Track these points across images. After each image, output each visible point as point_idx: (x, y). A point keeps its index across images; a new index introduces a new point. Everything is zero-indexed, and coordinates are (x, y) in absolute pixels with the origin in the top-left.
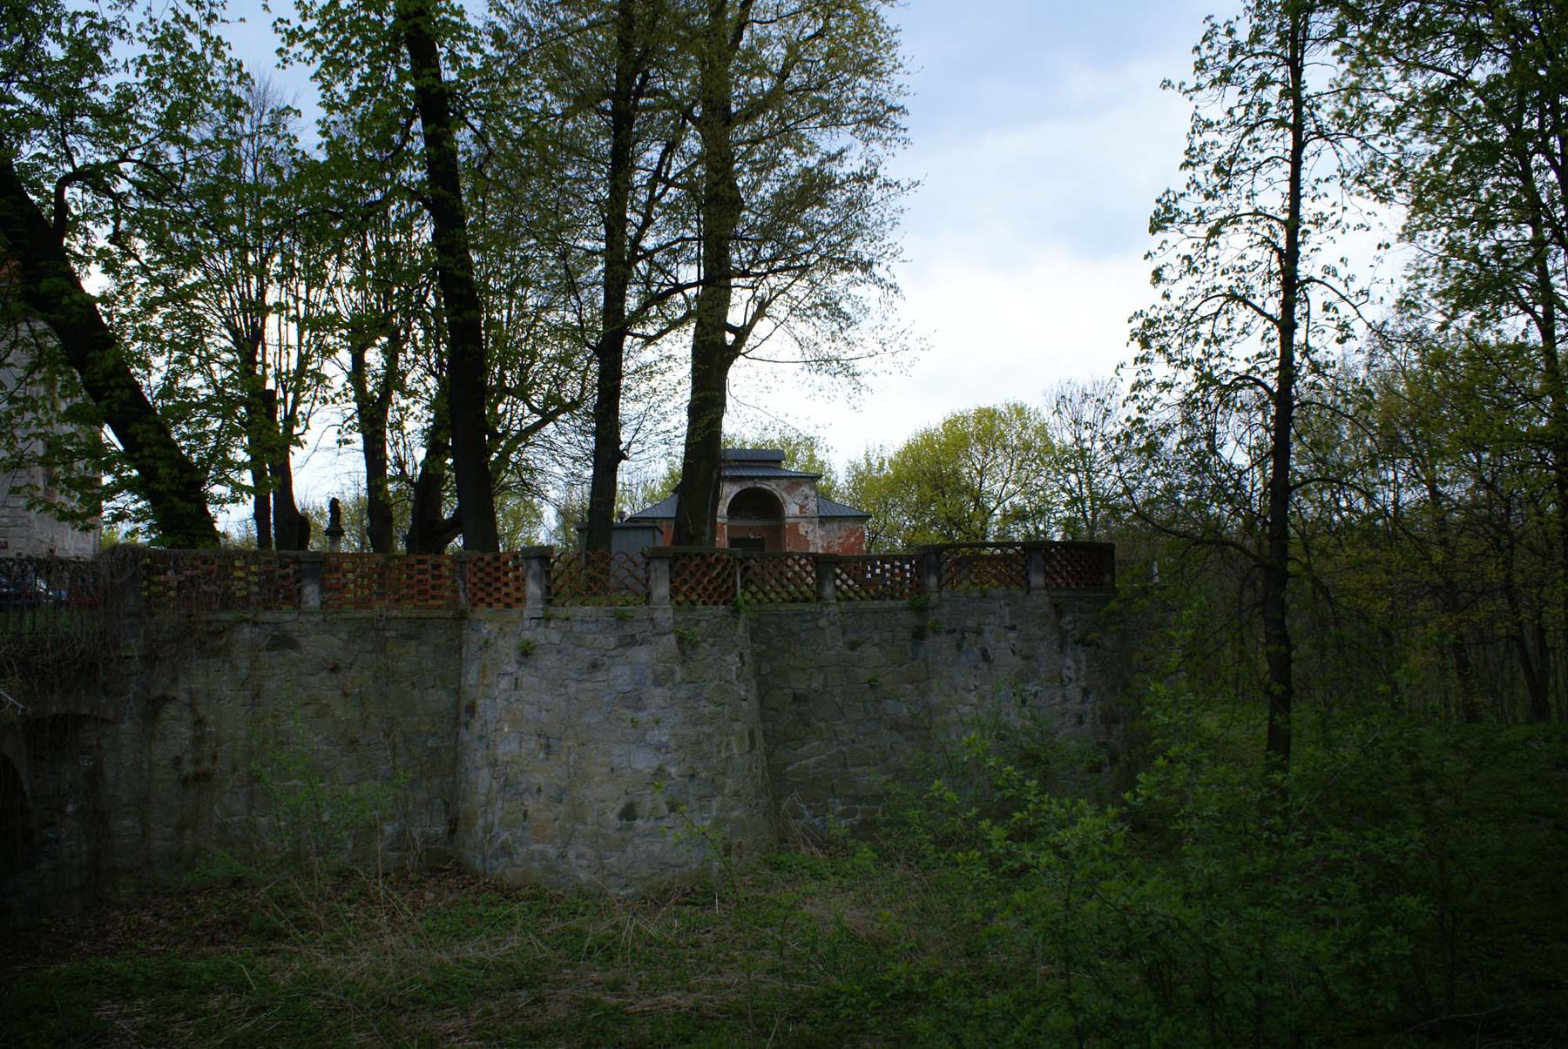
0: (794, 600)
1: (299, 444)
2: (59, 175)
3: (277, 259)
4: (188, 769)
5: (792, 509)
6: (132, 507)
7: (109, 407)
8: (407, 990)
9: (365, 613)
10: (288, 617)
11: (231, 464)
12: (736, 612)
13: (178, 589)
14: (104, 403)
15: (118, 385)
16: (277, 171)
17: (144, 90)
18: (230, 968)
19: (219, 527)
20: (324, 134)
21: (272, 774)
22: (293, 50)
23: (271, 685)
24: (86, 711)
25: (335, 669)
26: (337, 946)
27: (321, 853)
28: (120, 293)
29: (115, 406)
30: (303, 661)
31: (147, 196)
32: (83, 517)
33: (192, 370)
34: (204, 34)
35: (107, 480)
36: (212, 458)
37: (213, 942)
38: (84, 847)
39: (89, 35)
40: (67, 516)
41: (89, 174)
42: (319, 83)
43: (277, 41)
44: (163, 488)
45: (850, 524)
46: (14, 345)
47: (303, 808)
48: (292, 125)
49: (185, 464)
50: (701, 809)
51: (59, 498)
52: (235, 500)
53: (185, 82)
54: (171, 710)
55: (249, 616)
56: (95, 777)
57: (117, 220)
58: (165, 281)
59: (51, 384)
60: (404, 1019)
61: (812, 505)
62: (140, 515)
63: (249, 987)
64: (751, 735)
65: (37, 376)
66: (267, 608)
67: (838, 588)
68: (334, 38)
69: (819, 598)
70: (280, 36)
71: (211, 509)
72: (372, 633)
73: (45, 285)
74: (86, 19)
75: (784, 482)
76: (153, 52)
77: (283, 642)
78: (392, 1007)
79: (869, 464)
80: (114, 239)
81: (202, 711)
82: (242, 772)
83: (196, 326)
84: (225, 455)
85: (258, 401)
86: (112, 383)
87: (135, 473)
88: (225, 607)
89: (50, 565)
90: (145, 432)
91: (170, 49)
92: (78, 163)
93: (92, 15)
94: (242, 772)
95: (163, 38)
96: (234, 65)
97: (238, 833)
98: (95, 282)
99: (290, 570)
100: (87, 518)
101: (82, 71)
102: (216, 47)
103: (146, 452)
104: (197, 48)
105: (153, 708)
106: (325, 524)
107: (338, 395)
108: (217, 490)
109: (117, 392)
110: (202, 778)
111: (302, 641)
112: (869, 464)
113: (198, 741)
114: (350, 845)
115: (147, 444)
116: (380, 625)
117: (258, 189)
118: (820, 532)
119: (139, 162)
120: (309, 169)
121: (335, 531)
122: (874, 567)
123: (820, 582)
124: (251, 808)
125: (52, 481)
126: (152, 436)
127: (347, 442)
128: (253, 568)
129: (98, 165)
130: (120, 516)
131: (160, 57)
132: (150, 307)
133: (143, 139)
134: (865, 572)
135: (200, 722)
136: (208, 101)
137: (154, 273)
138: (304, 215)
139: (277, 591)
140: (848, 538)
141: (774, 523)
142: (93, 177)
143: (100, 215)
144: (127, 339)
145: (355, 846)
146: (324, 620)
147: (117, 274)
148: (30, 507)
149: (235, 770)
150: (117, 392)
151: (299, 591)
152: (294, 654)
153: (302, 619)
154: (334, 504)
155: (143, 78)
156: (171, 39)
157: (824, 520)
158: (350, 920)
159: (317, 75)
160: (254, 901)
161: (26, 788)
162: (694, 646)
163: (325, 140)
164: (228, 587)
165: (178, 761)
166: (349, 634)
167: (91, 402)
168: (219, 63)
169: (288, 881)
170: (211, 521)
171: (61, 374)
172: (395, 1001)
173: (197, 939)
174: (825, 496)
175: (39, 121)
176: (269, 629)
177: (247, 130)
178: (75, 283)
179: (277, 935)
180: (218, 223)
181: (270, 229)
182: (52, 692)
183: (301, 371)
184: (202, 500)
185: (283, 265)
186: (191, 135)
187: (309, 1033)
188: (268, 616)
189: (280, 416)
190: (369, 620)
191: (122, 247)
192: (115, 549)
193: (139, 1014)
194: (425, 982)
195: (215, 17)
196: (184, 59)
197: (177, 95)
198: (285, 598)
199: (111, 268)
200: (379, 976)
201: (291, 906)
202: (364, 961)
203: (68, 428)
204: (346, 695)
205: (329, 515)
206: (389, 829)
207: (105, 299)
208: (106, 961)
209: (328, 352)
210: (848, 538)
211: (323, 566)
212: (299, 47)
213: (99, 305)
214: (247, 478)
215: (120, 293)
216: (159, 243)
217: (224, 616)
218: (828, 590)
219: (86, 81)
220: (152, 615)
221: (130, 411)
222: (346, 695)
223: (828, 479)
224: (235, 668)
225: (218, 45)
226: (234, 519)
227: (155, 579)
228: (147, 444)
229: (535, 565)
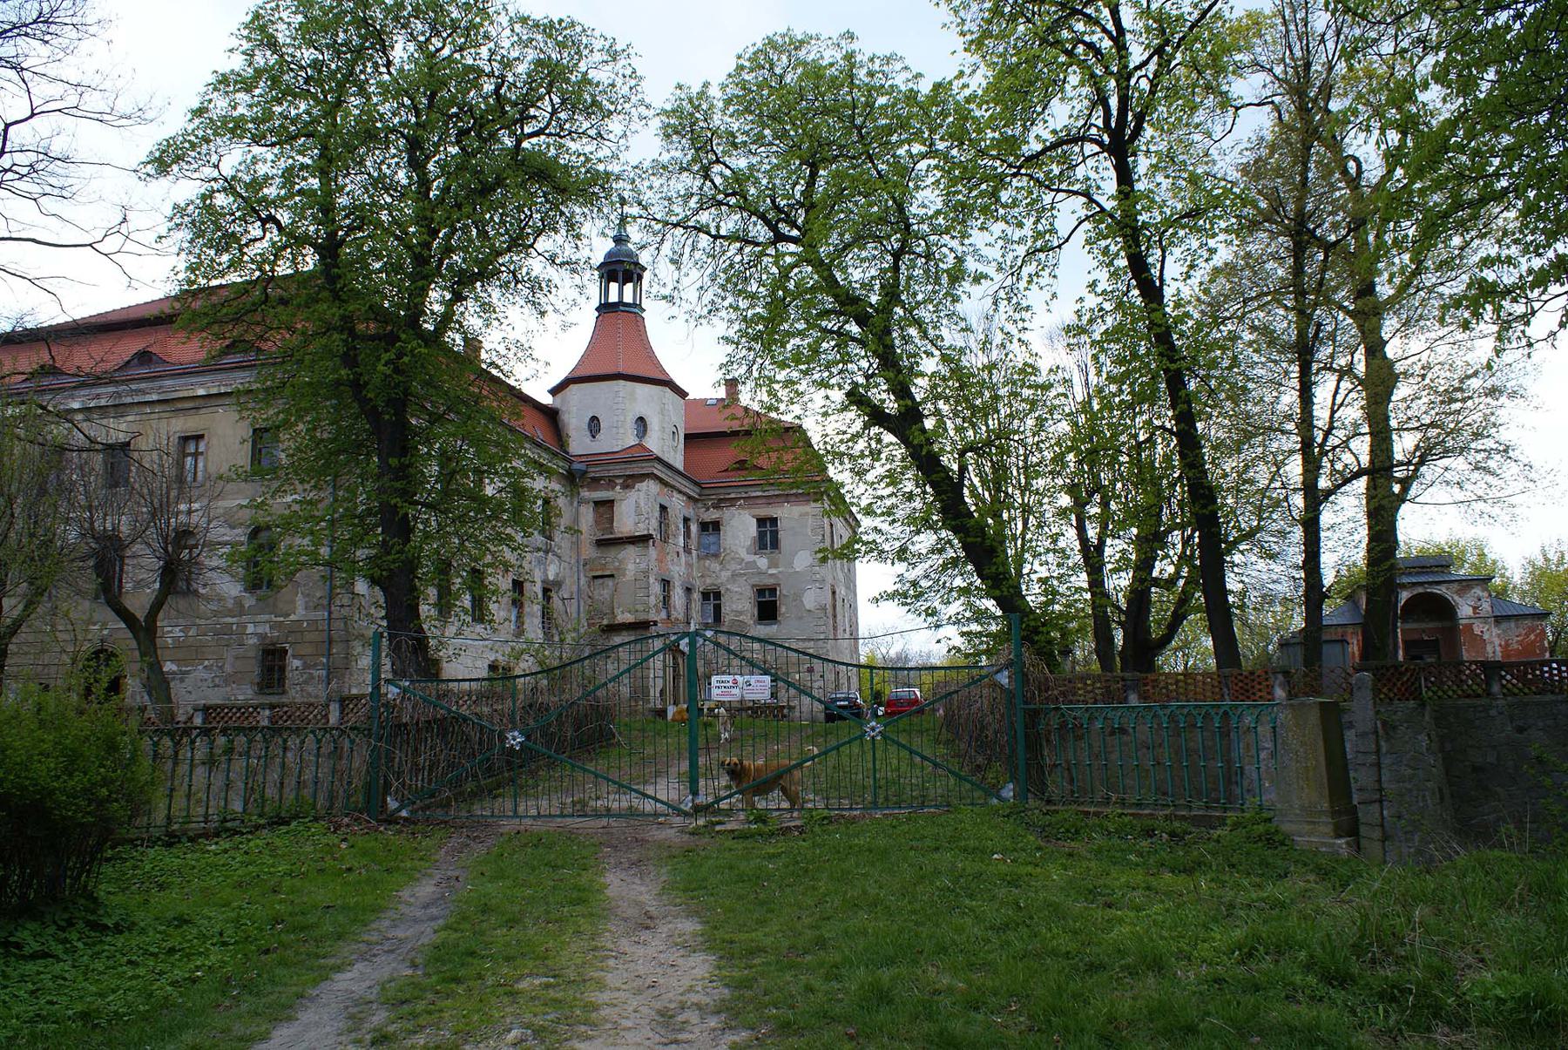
0: (1468, 696)
5: (1465, 610)
12: (1423, 705)
45: (1528, 622)
50: (1407, 840)
61: (1486, 606)
64: (1440, 790)
67: (1503, 686)
69: (1489, 694)
75: (1456, 585)
79: (1547, 560)
112: (1547, 560)
118: (1495, 631)
122: (1534, 670)
123: (1488, 682)
134: (1526, 673)
140: (1527, 635)
141: (1447, 624)
157: (1499, 620)
162: (1394, 728)
174: (1502, 593)
210: (1527, 635)
218: (1496, 688)
223: (1502, 576)
229: (1280, 677)
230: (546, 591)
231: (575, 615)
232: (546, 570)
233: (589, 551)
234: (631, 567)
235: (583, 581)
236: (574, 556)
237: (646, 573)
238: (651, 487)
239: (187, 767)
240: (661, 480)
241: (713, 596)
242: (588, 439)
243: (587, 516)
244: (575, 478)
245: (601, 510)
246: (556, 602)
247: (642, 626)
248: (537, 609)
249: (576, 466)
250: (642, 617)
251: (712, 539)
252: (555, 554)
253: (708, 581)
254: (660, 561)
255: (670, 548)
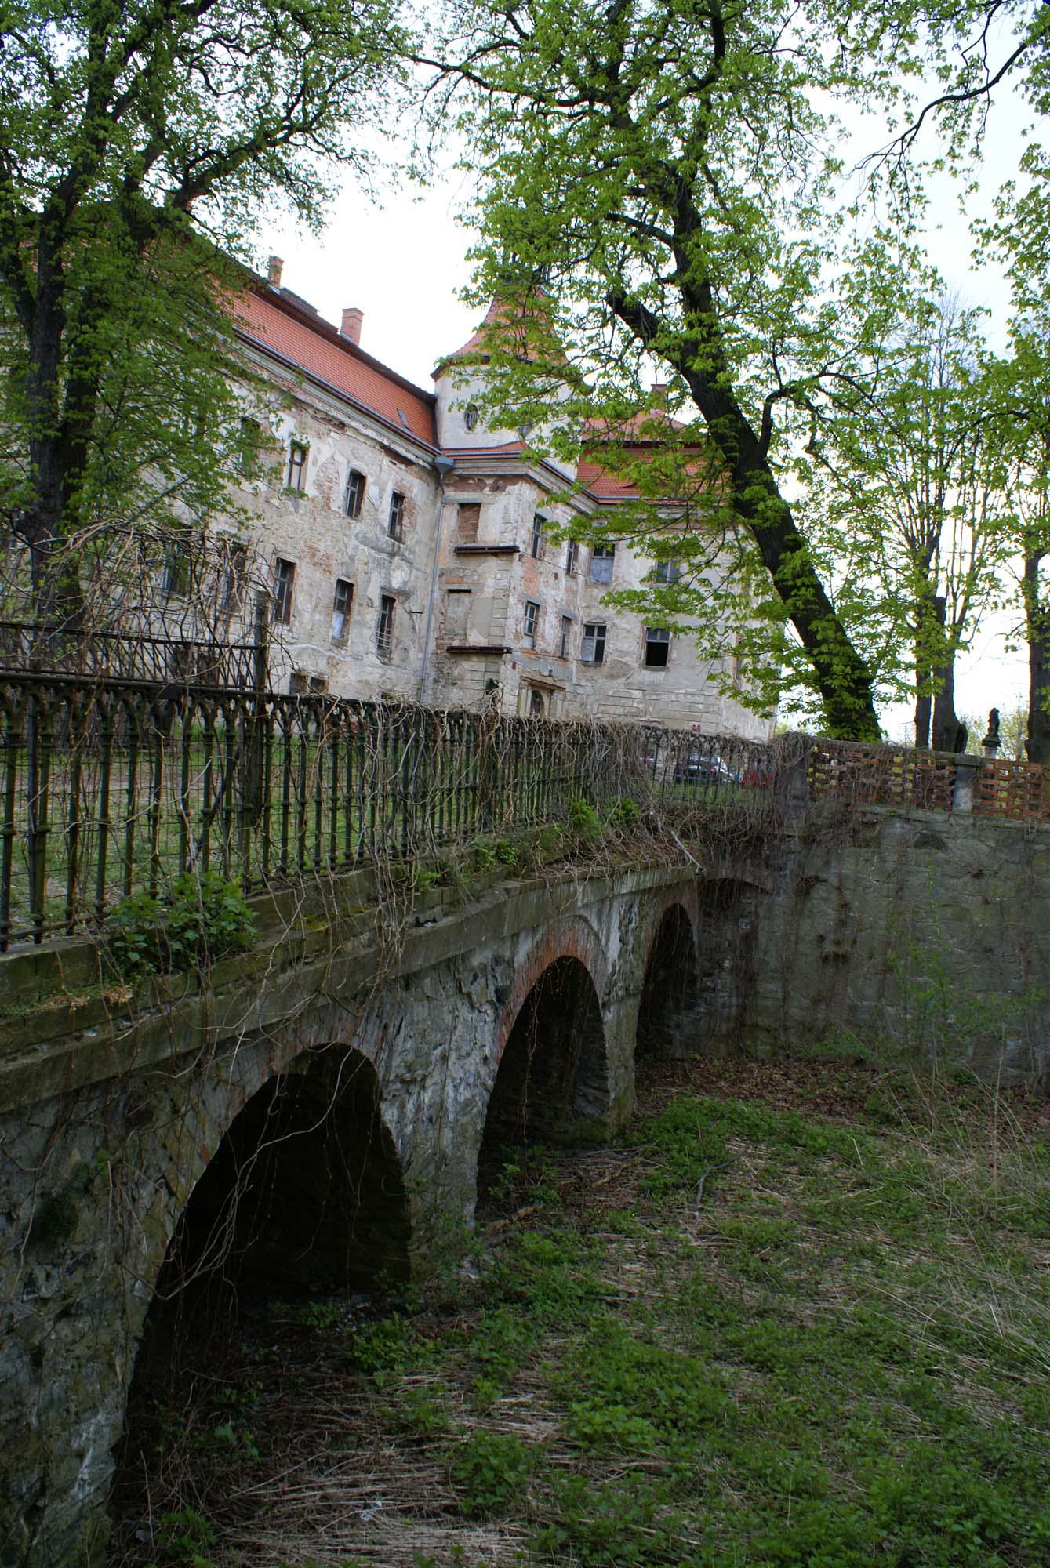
1: (965, 646)
2: (768, 393)
3: (958, 461)
4: (829, 948)
6: (807, 699)
7: (794, 605)
8: (1008, 1208)
9: (1017, 823)
10: (939, 818)
11: (897, 664)
13: (840, 778)
14: (790, 601)
15: (803, 585)
16: (963, 374)
17: (845, 306)
18: (843, 1139)
19: (882, 724)
20: (1014, 333)
21: (905, 967)
22: (987, 250)
23: (915, 881)
24: (749, 880)
25: (979, 875)
26: (943, 1147)
27: (942, 1053)
28: (812, 500)
29: (800, 604)
30: (948, 862)
31: (841, 406)
32: (763, 705)
33: (870, 573)
34: (902, 246)
35: (786, 672)
36: (882, 654)
37: (830, 1112)
38: (734, 1000)
39: (802, 262)
40: (749, 703)
41: (793, 390)
42: (1012, 281)
43: (972, 242)
44: (835, 683)
46: (721, 547)
47: (931, 1005)
48: (983, 326)
49: (856, 663)
51: (746, 687)
52: (899, 700)
53: (883, 294)
54: (820, 891)
55: (902, 812)
56: (749, 939)
57: (813, 429)
58: (853, 488)
59: (746, 581)
60: (1000, 1235)
62: (813, 707)
63: (857, 1161)
65: (737, 575)
66: (920, 806)
68: (1031, 231)
70: (975, 237)
71: (876, 705)
72: (1021, 844)
73: (748, 493)
74: (801, 247)
76: (856, 269)
77: (931, 841)
78: (990, 1219)
80: (812, 448)
81: (848, 896)
82: (878, 960)
83: (875, 526)
84: (893, 656)
85: (930, 604)
86: (799, 582)
87: (811, 667)
88: (881, 800)
89: (732, 745)
90: (824, 629)
91: (870, 264)
92: (785, 381)
93: (807, 243)
94: (878, 960)
95: (866, 255)
96: (929, 272)
97: (866, 1017)
98: (791, 489)
99: (946, 772)
100: (764, 706)
101: (793, 295)
102: (913, 257)
103: (824, 648)
104: (895, 261)
105: (806, 886)
106: (982, 733)
107: (1008, 601)
108: (883, 689)
109: (803, 591)
110: (841, 959)
111: (950, 843)
113: (842, 923)
114: (970, 1051)
115: (825, 641)
116: (1031, 837)
117: (942, 395)
119: (837, 375)
120: (996, 372)
121: (992, 742)
124: (881, 996)
125: (741, 671)
126: (830, 634)
127: (1014, 649)
128: (912, 766)
129: (801, 382)
130: (794, 707)
131: (861, 273)
132: (836, 512)
133: (842, 353)
135: (845, 906)
136: (902, 310)
137: (843, 480)
138: (989, 417)
139: (931, 791)
142: (793, 393)
143: (799, 427)
144: (814, 542)
145: (975, 1054)
146: (974, 825)
147: (811, 482)
148: (722, 693)
149: (871, 957)
150: (803, 591)
151: (952, 793)
152: (941, 855)
153: (951, 820)
154: (994, 715)
155: (845, 295)
156: (873, 256)
158: (961, 1124)
159: (1011, 273)
160: (873, 1084)
161: (695, 939)
163: (1014, 339)
164: (885, 782)
165: (821, 939)
166: (997, 841)
167: (779, 600)
168: (914, 273)
169: (905, 1072)
170: (874, 720)
171: (757, 574)
172: (993, 1215)
173: (817, 1105)
175: (757, 346)
176: (919, 826)
177: (936, 337)
178: (772, 489)
179: (888, 1120)
180: (900, 431)
181: (953, 434)
182: (724, 858)
183: (973, 577)
184: (868, 697)
185: (962, 469)
186: (884, 344)
187: (906, 1219)
188: (920, 814)
189: (948, 622)
190: (1021, 830)
191: (816, 456)
192: (787, 736)
193: (760, 1158)
194: (1027, 1204)
195: (913, 228)
196: (883, 272)
197: (875, 307)
198: (938, 798)
199: (805, 476)
200: (982, 1185)
201: (907, 1097)
202: (970, 1166)
203: (756, 624)
204: (986, 902)
205: (987, 725)
206: (1011, 1044)
207: (797, 506)
208: (740, 1105)
209: (1003, 555)
211: (979, 773)
212: (993, 245)
213: (793, 512)
214: (911, 678)
215: (812, 500)
216: (850, 453)
217: (878, 809)
219: (796, 305)
220: (814, 800)
221: (808, 606)
222: (986, 902)
224: (882, 860)
225: (913, 255)
226: (897, 721)
227: (820, 766)
228: (825, 641)
230: (388, 601)
231: (424, 632)
232: (388, 577)
233: (448, 561)
234: (490, 582)
235: (437, 594)
236: (431, 564)
237: (506, 592)
238: (524, 493)
239: (324, 797)
240: (540, 486)
241: (596, 631)
242: (462, 429)
243: (451, 516)
244: (439, 475)
245: (467, 514)
246: (399, 612)
247: (495, 652)
248: (372, 616)
249: (441, 460)
250: (496, 642)
251: (604, 564)
252: (404, 559)
253: (594, 613)
254: (528, 580)
255: (546, 567)
